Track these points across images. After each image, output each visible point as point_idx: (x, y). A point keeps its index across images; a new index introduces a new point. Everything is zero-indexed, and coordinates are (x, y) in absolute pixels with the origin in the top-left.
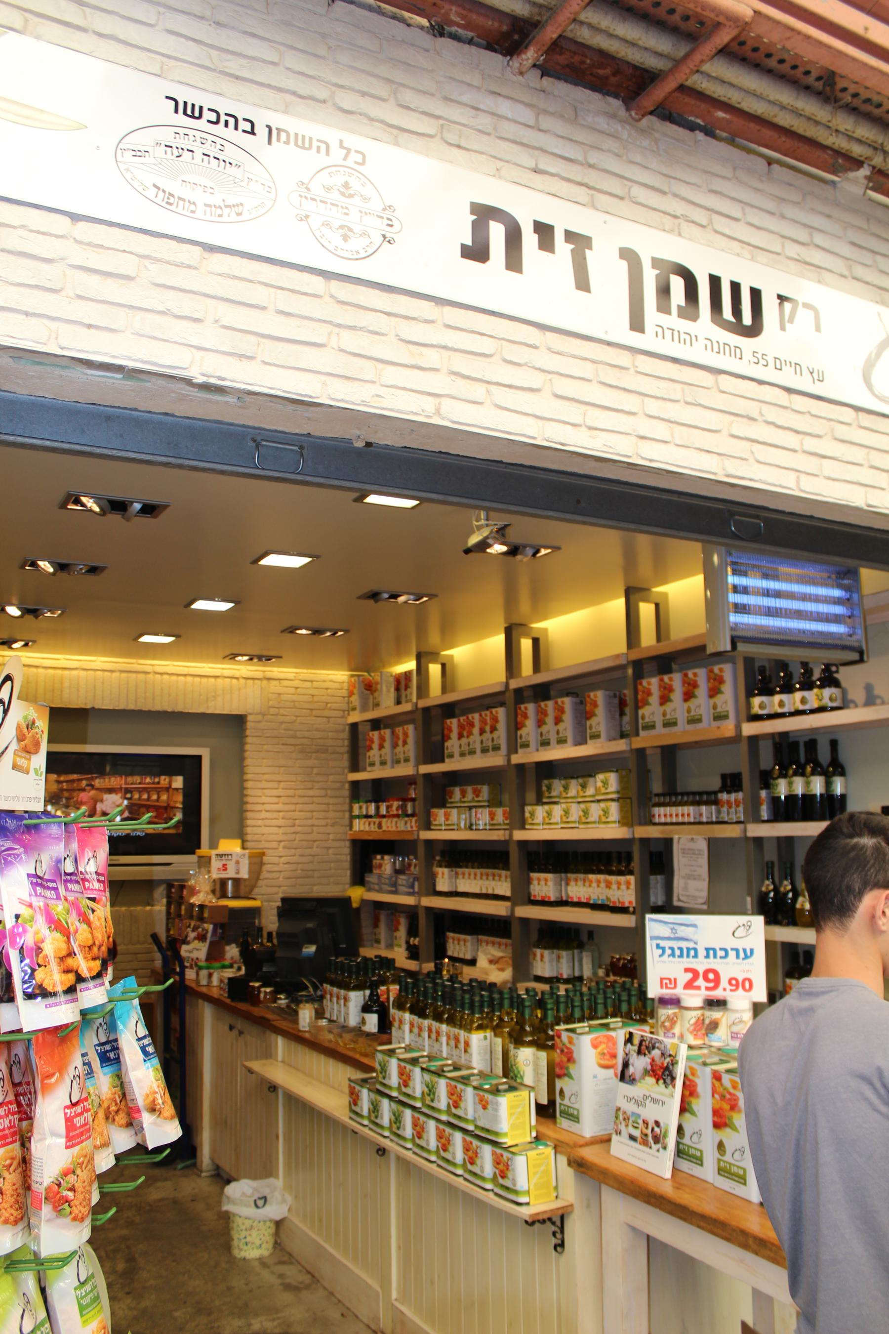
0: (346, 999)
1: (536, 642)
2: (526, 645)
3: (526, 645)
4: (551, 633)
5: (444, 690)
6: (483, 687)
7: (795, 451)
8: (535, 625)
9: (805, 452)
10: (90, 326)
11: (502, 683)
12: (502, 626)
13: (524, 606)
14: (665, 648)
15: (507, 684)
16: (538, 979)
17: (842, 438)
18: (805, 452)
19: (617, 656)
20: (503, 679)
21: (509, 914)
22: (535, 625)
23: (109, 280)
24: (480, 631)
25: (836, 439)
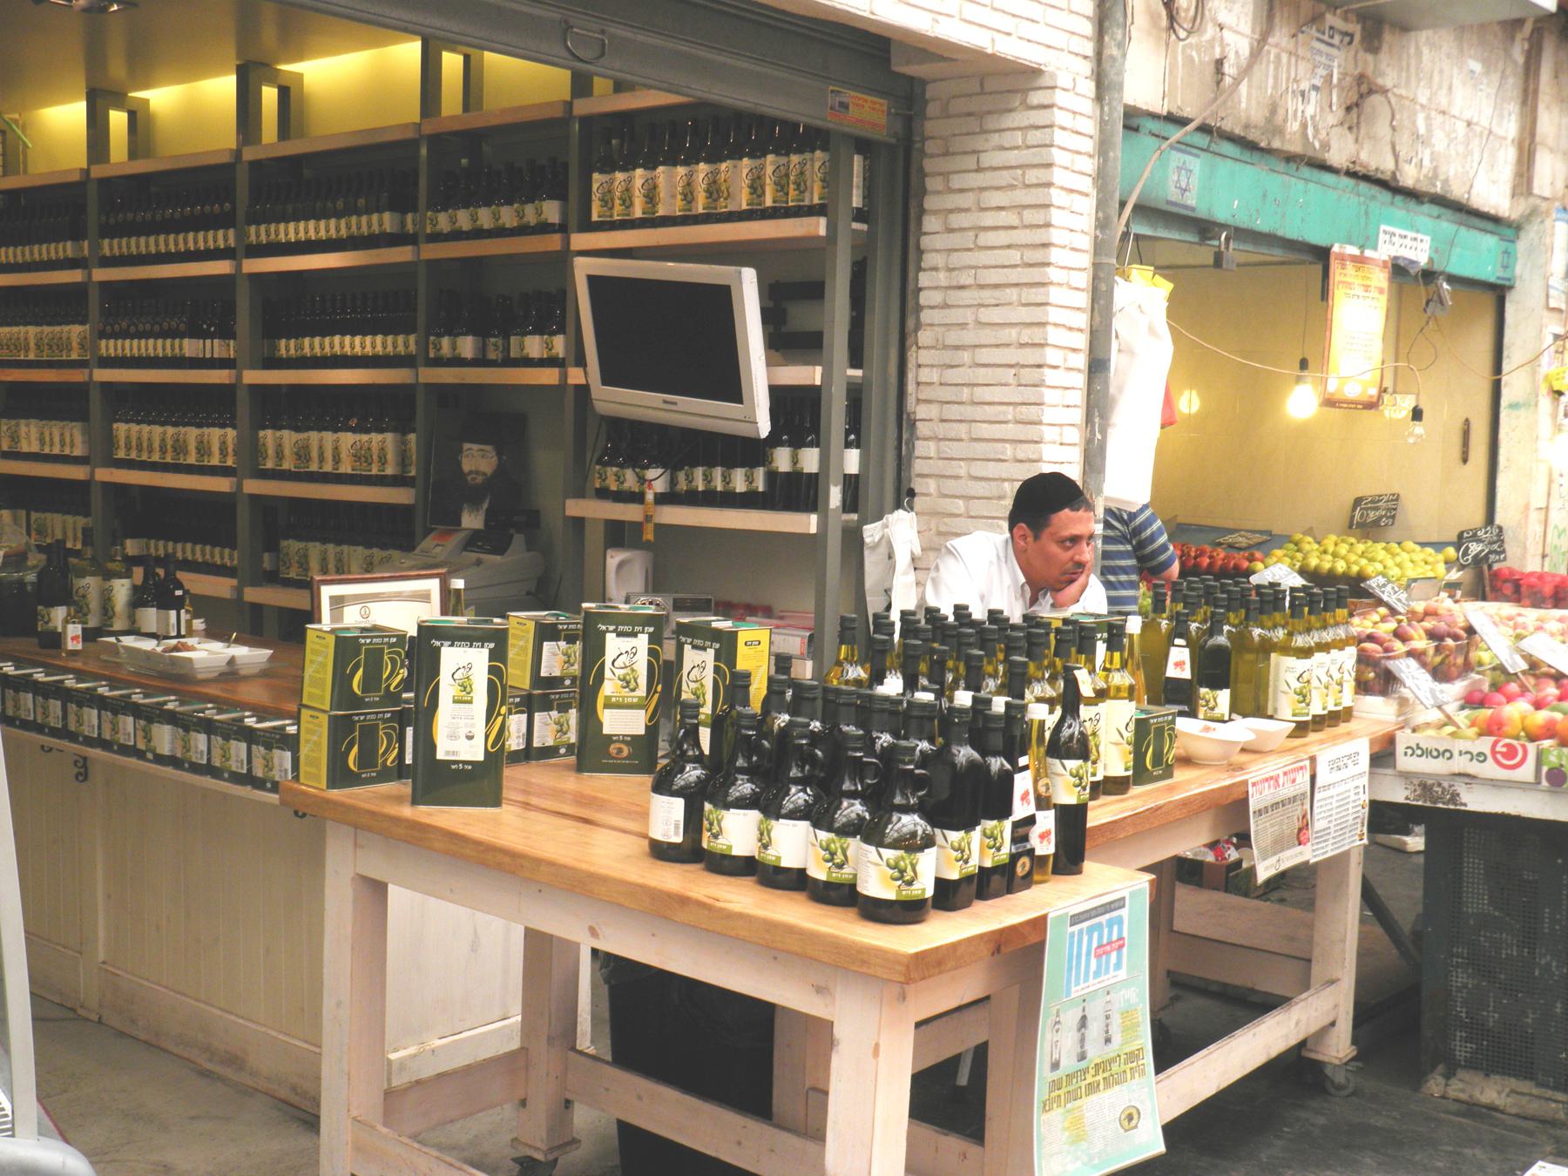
0: (774, 202)
1: (284, 93)
2: (269, 95)
3: (269, 95)
4: (306, 80)
5: (133, 153)
6: (208, 153)
7: (1062, 50)
8: (283, 67)
9: (1070, 52)
10: (1049, 47)
11: (231, 150)
12: (234, 63)
13: (269, 35)
14: (475, 121)
15: (238, 153)
16: (65, 717)
17: (969, 18)
18: (1070, 52)
19: (406, 126)
20: (232, 142)
21: (234, 490)
22: (283, 67)
23: (1238, 163)
24: (193, 66)
25: (965, 21)
